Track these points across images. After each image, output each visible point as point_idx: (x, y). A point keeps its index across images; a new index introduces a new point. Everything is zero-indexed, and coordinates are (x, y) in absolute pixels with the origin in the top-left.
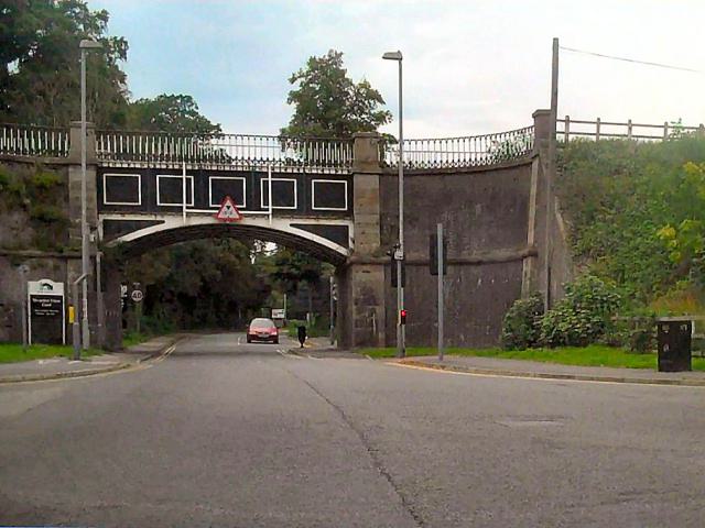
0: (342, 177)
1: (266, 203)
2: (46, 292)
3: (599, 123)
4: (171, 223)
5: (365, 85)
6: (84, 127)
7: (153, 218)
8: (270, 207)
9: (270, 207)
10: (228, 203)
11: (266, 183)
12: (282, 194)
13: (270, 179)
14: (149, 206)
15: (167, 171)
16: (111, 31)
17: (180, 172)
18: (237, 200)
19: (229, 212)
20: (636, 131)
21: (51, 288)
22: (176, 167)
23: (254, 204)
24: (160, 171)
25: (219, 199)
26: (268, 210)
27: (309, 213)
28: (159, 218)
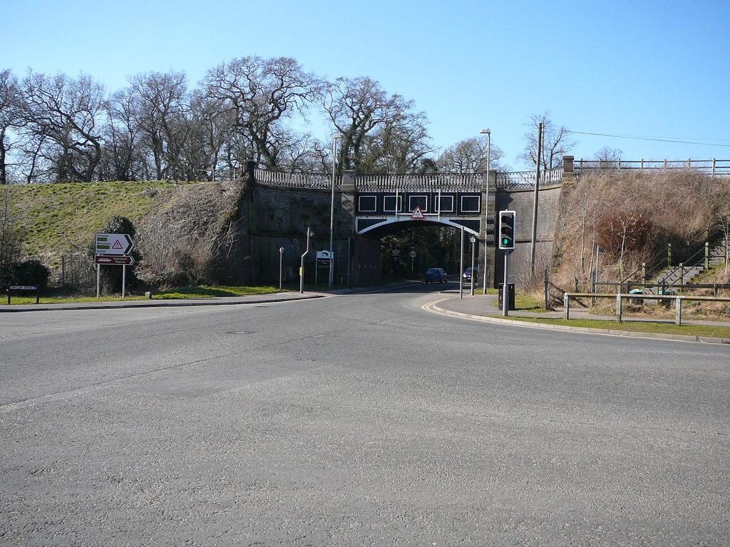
0: (478, 194)
1: (437, 209)
2: (325, 256)
3: (666, 162)
4: (390, 220)
5: (85, 84)
6: (618, 299)
7: (381, 218)
8: (439, 211)
9: (439, 211)
10: (418, 209)
11: (438, 198)
12: (445, 204)
13: (439, 196)
14: (380, 212)
15: (389, 194)
16: (156, 72)
17: (441, 214)
18: (422, 208)
19: (417, 214)
20: (693, 165)
21: (327, 254)
22: (394, 191)
23: (431, 210)
24: (386, 194)
25: (413, 208)
26: (437, 213)
27: (460, 214)
28: (384, 218)
